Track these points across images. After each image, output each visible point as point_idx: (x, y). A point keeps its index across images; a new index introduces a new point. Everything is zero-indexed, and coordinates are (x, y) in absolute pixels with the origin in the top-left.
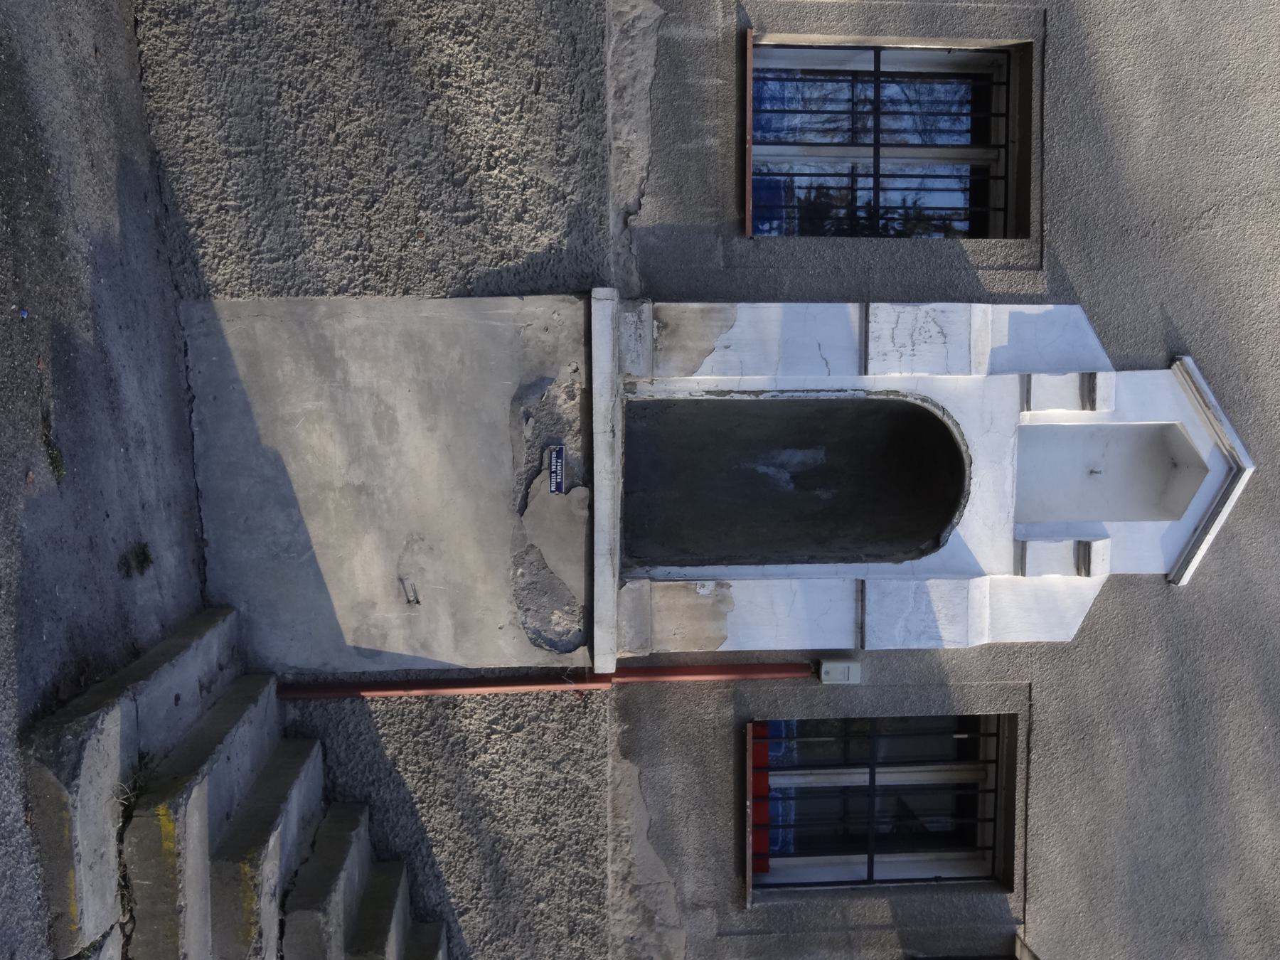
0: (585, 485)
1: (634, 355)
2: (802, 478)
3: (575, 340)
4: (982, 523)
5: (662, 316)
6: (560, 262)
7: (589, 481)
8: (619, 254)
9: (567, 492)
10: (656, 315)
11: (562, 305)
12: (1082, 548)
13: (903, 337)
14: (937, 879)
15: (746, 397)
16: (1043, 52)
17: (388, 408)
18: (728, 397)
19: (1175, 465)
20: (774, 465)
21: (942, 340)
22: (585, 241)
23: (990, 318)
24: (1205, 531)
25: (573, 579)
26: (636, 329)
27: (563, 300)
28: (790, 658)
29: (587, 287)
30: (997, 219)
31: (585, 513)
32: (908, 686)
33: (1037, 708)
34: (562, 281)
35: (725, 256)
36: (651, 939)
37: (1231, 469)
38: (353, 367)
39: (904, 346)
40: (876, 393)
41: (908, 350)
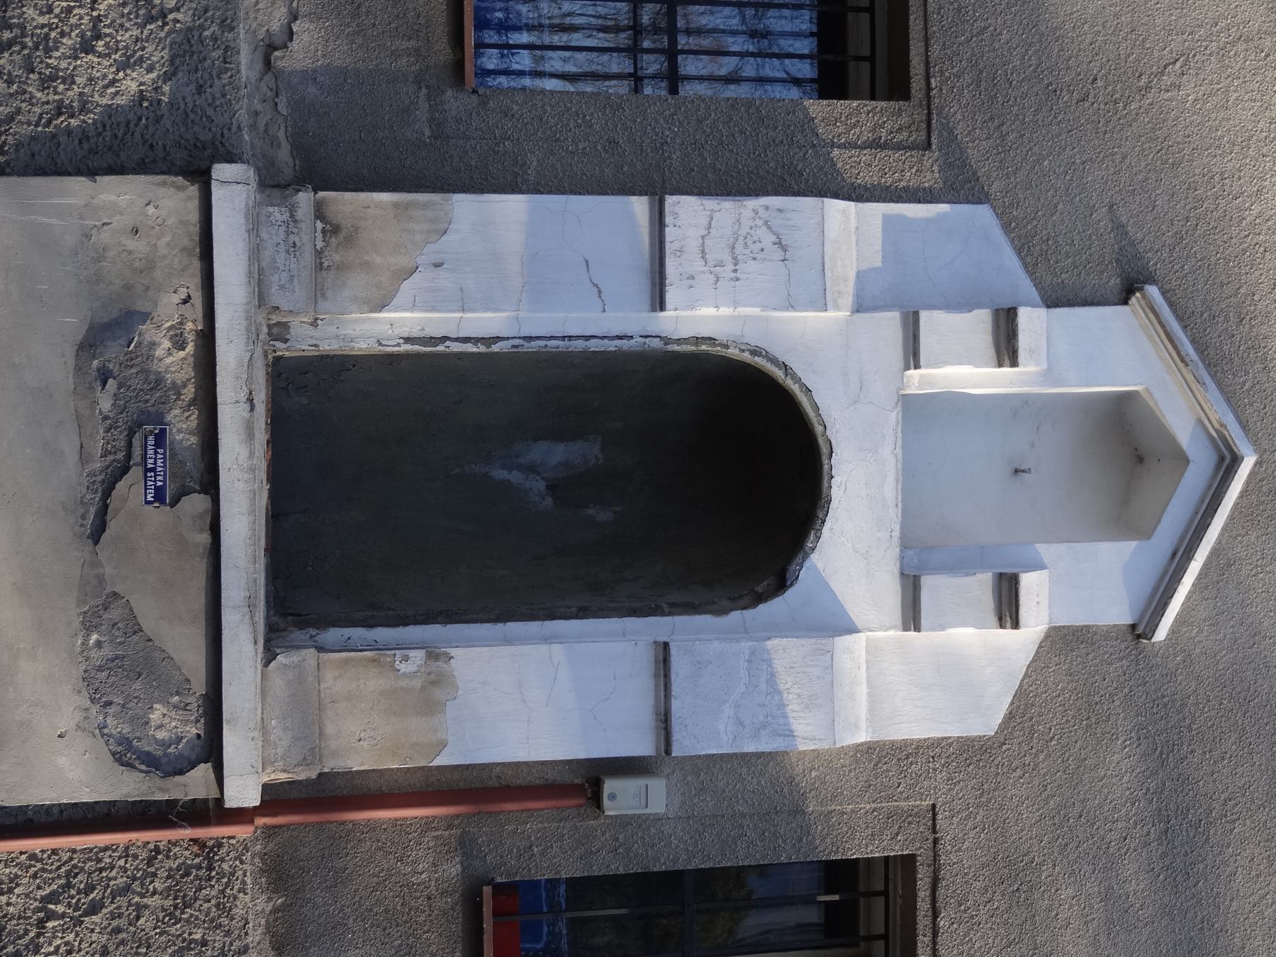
0: (204, 491)
1: (285, 276)
2: (564, 488)
4: (852, 546)
7: (210, 484)
8: (257, 114)
10: (320, 212)
12: (1005, 585)
13: (718, 251)
15: (470, 348)
18: (440, 348)
20: (520, 467)
21: (779, 254)
26: (287, 233)
27: (164, 184)
29: (203, 165)
30: (830, 304)
31: (205, 538)
32: (743, 815)
33: (946, 845)
35: (431, 120)
37: (1222, 458)
39: (720, 264)
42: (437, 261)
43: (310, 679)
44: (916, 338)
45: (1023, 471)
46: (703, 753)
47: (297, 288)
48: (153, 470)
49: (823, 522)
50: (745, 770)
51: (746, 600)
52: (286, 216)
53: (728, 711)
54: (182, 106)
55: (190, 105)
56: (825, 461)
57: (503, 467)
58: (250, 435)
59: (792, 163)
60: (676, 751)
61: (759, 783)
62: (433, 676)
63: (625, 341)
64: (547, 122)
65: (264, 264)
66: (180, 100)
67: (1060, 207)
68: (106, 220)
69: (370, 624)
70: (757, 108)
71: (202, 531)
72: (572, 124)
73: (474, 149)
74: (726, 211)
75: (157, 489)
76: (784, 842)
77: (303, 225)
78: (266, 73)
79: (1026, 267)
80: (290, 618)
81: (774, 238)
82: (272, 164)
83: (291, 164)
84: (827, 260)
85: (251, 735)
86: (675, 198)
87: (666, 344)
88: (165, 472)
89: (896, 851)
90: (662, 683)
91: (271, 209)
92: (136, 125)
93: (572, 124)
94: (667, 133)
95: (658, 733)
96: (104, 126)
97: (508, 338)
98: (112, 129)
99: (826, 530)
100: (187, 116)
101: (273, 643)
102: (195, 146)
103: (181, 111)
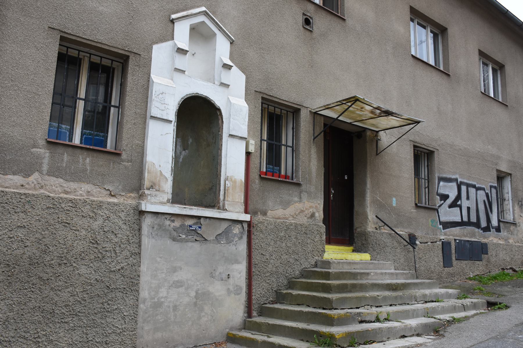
0: (200, 219)
5: (149, 187)
7: (199, 218)
10: (149, 189)
11: (146, 221)
14: (293, 129)
16: (65, 32)
17: (174, 283)
21: (164, 94)
22: (123, 211)
24: (221, 28)
25: (224, 225)
31: (208, 219)
35: (127, 162)
36: (306, 212)
38: (161, 295)
41: (167, 106)
44: (179, 70)
58: (192, 209)
60: (247, 137)
89: (260, 101)
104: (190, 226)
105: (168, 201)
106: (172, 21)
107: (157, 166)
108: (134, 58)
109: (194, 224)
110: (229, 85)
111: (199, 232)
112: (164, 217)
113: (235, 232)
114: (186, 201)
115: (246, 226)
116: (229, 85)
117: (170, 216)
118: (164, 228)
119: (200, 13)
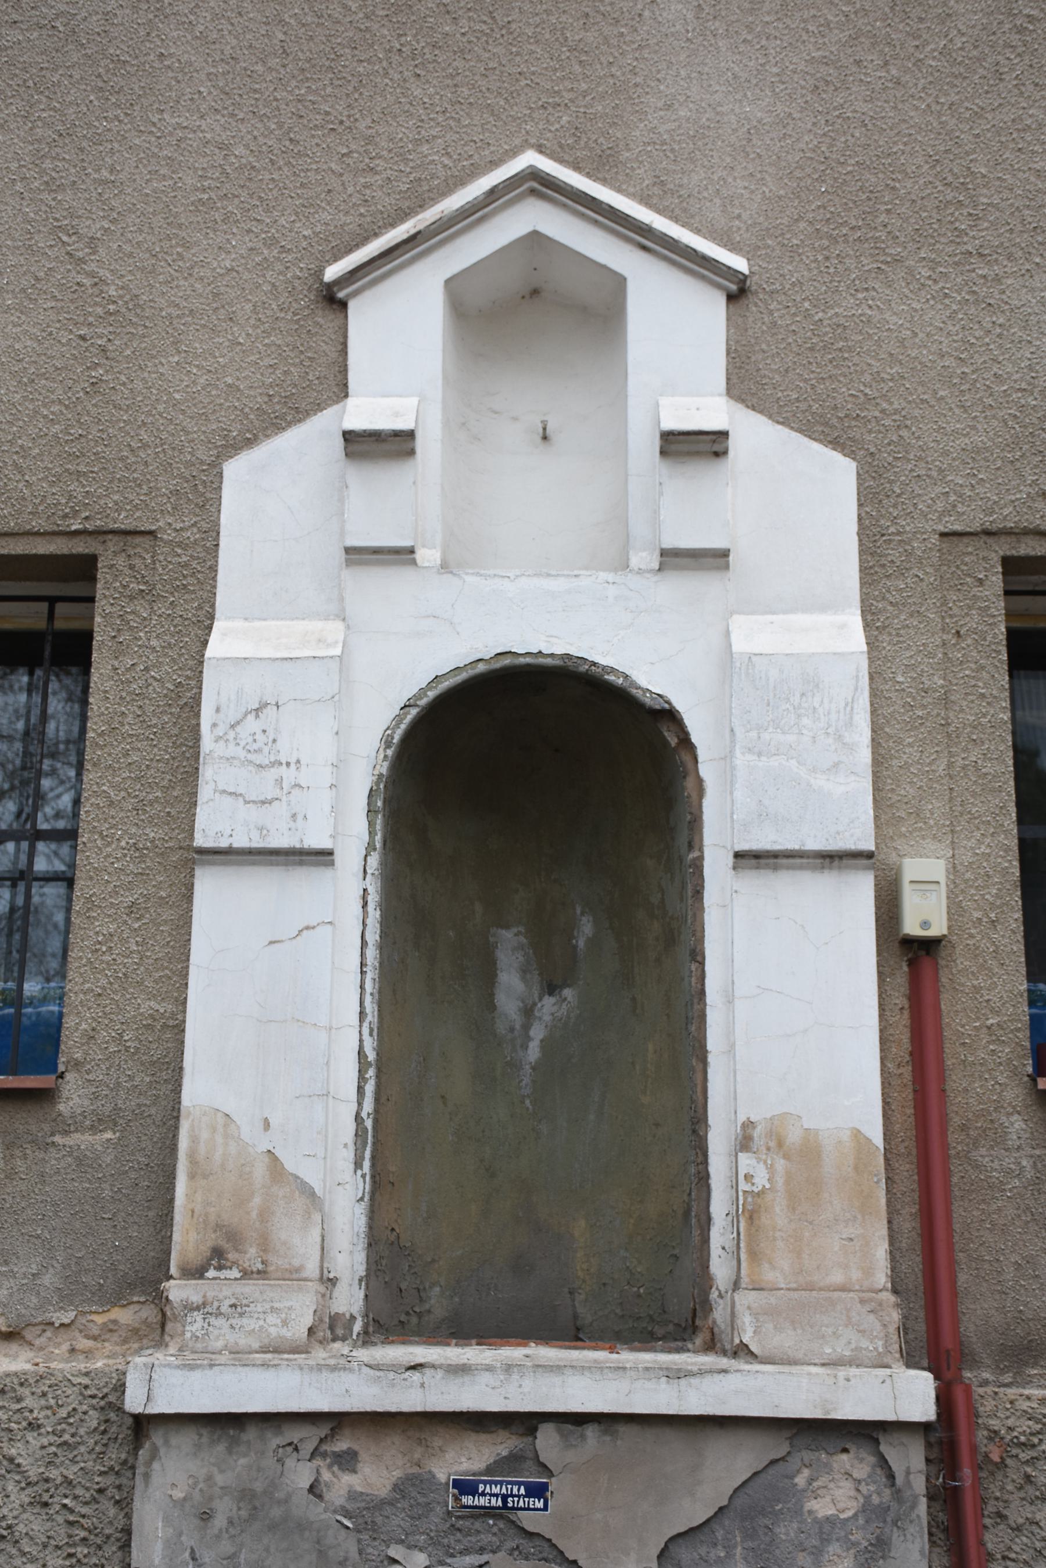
0: (532, 1432)
1: (272, 1319)
2: (552, 974)
3: (230, 1451)
5: (195, 1258)
6: (70, 1483)
7: (527, 1423)
8: (73, 1350)
9: (545, 1469)
10: (197, 1272)
11: (156, 1479)
12: (673, 447)
13: (264, 785)
15: (370, 1088)
18: (369, 1124)
19: (535, 292)
20: (526, 1027)
21: (271, 711)
22: (33, 1426)
23: (239, 624)
24: (645, 230)
25: (730, 1466)
26: (219, 1314)
27: (147, 1476)
28: (899, 999)
29: (129, 1421)
30: (66, 618)
31: (591, 1431)
32: (950, 765)
33: (994, 520)
34: (109, 1480)
35: (93, 1129)
37: (533, 192)
39: (279, 781)
40: (372, 833)
41: (289, 775)
42: (260, 1125)
43: (773, 1300)
44: (376, 551)
45: (545, 429)
46: (871, 812)
47: (288, 1304)
48: (505, 1498)
49: (594, 664)
50: (894, 762)
51: (686, 757)
52: (198, 1316)
53: (820, 781)
54: (53, 1449)
55: (52, 1438)
56: (522, 660)
57: (525, 1047)
59: (166, 696)
60: (870, 846)
61: (910, 745)
62: (772, 1144)
63: (370, 898)
64: (104, 988)
65: (256, 1345)
66: (44, 1452)
67: (229, 380)
68: (187, 1554)
69: (707, 1221)
70: (99, 735)
71: (583, 1437)
72: (107, 958)
73: (131, 1078)
74: (214, 776)
75: (528, 1495)
76: (984, 715)
77: (210, 1295)
78: (23, 1337)
79: (300, 421)
80: (698, 1322)
81: (251, 718)
82: (135, 1331)
83: (137, 1307)
84: (279, 655)
85: (841, 1382)
86: (196, 835)
87: (375, 849)
88: (509, 1483)
89: (997, 581)
90: (784, 861)
91: (188, 1335)
92: (72, 1511)
93: (107, 958)
94: (123, 844)
95: (847, 867)
96: (70, 1555)
97: (361, 1041)
98: (75, 1545)
99: (603, 661)
100: (65, 1443)
101: (728, 1347)
102: (104, 1432)
103: (59, 1452)
104: (465, 1487)
105: (330, 1328)
106: (333, 300)
107: (248, 1130)
108: (121, 561)
109: (489, 1470)
110: (725, 554)
111: (527, 1520)
112: (275, 1441)
113: (822, 1507)
114: (580, 1298)
115: (910, 1461)
116: (725, 554)
117: (323, 1431)
118: (276, 1512)
119: (493, 194)
